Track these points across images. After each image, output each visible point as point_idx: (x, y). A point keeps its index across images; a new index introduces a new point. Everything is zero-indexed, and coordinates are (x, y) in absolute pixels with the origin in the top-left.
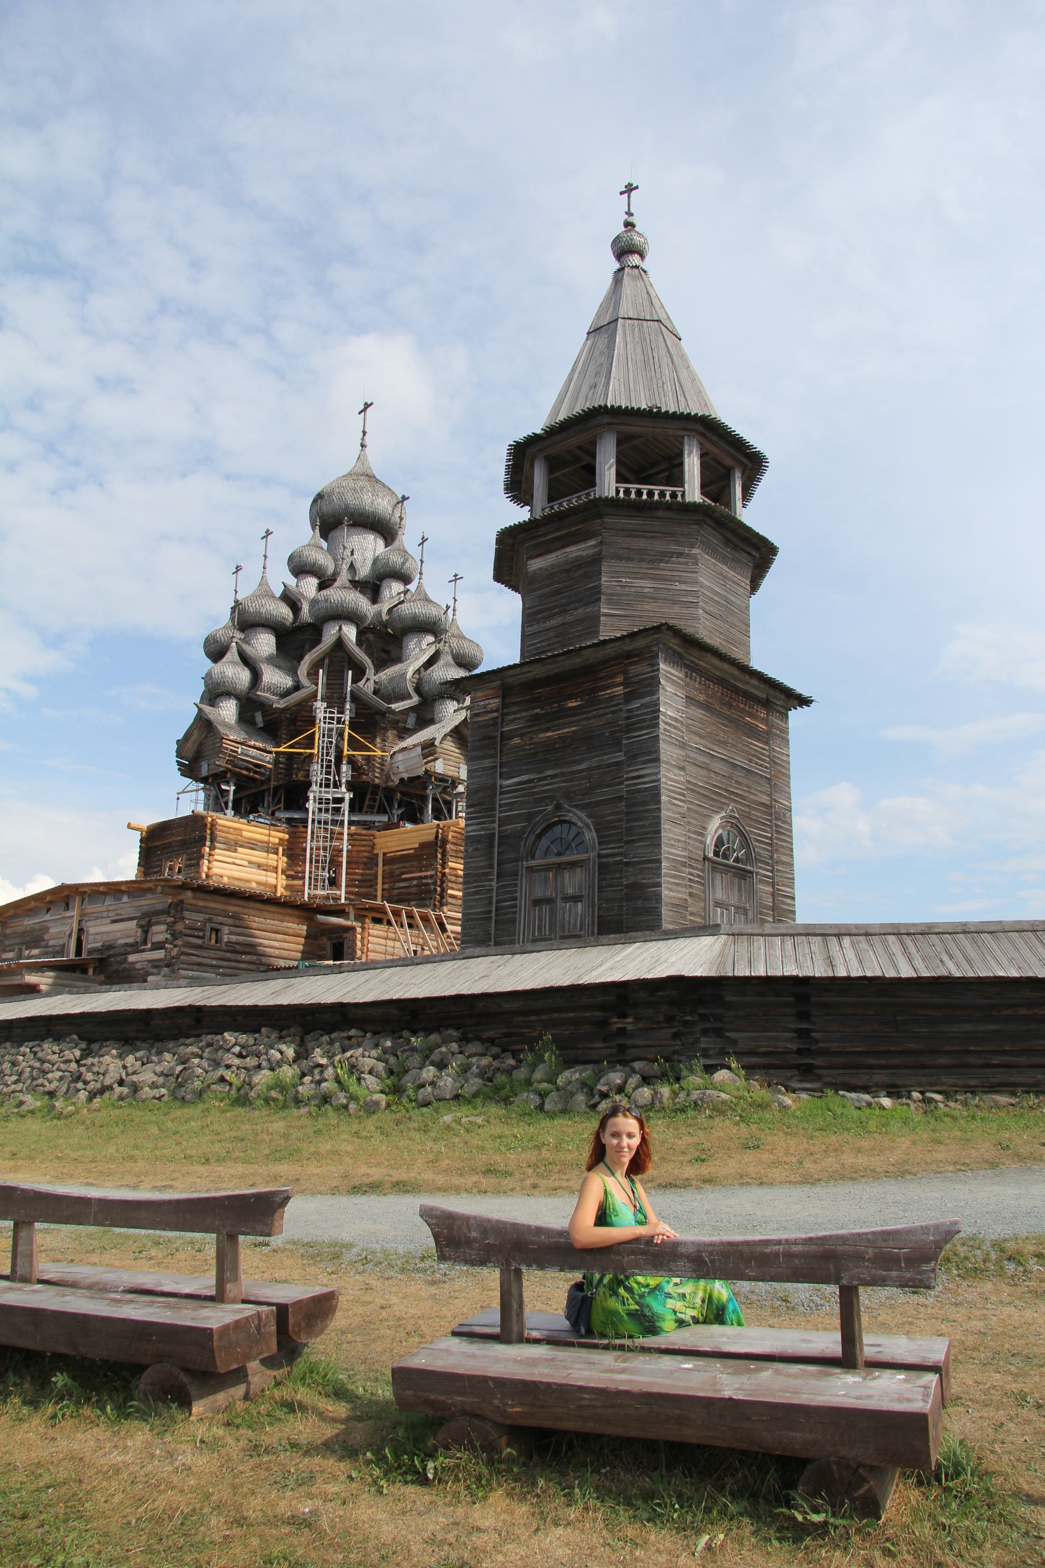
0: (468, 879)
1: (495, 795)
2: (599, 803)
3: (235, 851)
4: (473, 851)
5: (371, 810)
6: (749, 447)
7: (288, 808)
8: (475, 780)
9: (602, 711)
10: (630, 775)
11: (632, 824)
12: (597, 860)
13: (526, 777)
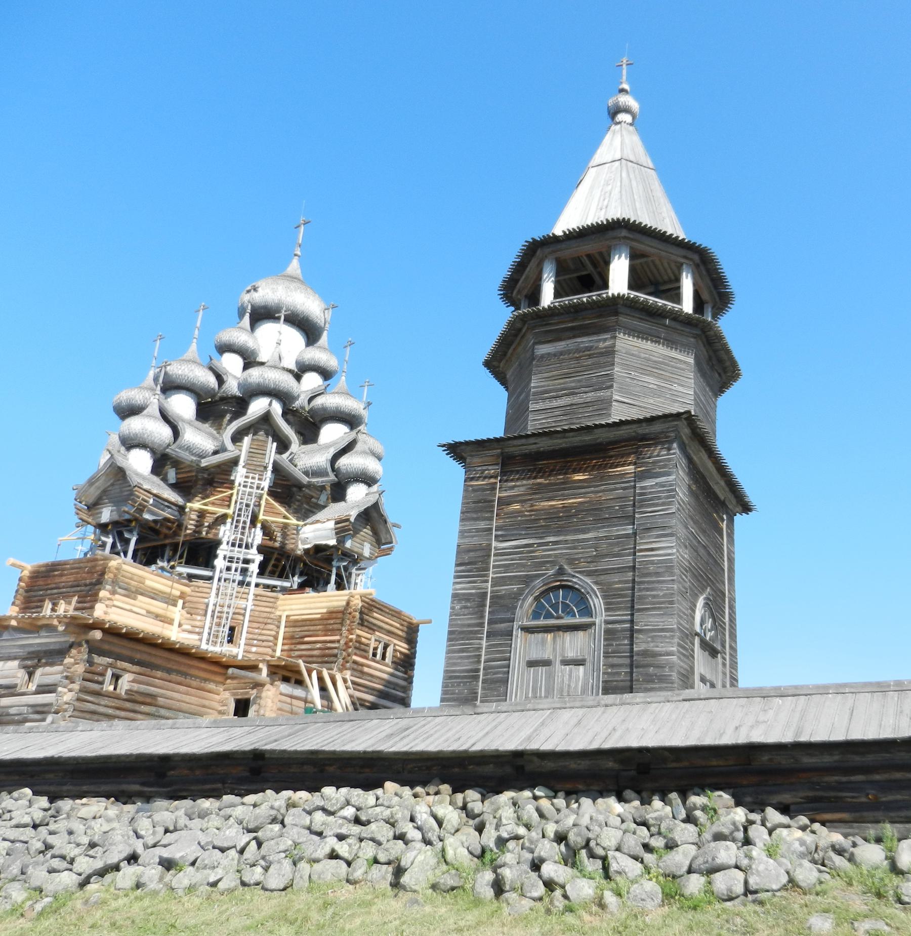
0: (453, 636)
1: (489, 556)
2: (606, 572)
3: (135, 599)
4: (461, 608)
5: (272, 575)
6: (725, 287)
7: (190, 562)
8: (466, 540)
9: (612, 486)
10: (642, 547)
11: (644, 593)
12: (603, 626)
13: (531, 541)
